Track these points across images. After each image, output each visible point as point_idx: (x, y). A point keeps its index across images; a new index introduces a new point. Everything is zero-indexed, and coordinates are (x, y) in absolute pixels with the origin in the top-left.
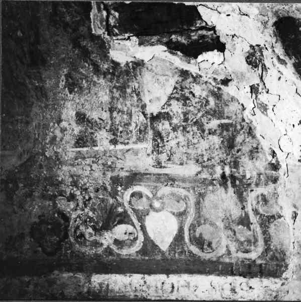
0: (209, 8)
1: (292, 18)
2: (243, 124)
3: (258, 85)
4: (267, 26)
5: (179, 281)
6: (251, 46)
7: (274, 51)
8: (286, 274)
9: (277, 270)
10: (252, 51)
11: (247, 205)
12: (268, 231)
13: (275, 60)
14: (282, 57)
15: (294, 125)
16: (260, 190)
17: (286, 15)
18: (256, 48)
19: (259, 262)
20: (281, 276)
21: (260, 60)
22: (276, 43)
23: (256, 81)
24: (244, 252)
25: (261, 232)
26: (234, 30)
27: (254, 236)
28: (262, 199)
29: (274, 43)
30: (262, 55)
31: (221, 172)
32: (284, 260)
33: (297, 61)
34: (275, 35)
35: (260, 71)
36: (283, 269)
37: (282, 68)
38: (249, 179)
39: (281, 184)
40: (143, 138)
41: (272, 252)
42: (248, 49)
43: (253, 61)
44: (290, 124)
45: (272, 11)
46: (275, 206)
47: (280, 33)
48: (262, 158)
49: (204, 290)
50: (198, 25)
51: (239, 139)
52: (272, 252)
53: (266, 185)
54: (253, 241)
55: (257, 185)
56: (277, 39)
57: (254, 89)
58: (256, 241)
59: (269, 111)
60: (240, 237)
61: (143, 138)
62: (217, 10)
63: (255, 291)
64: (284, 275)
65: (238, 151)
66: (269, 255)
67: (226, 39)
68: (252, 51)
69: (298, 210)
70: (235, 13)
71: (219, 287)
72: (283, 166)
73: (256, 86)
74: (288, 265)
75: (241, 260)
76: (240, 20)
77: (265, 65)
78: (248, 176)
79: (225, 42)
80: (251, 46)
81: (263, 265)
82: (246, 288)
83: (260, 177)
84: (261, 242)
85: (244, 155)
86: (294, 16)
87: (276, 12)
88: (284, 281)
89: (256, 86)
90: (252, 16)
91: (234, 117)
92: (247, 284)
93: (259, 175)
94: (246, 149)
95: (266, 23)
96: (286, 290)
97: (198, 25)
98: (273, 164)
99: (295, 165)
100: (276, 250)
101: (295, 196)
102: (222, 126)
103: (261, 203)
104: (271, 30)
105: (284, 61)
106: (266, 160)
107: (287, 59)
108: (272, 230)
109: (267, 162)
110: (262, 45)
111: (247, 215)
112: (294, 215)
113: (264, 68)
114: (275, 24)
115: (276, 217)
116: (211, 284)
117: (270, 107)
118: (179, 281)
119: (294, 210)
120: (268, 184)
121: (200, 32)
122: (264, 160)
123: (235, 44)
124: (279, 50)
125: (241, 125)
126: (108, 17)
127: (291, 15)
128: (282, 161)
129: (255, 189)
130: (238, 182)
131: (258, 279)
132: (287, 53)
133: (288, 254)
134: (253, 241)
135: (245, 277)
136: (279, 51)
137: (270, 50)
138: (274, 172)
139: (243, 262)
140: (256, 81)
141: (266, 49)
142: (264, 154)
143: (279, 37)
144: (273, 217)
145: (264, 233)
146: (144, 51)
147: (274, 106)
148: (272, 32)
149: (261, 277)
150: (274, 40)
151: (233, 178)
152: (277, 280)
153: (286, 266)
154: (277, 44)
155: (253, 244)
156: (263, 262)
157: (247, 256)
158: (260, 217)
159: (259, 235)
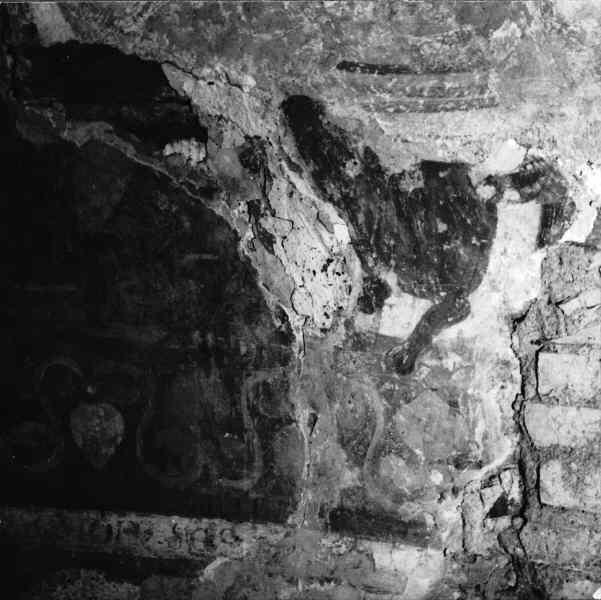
0: (179, 68)
1: (307, 98)
2: (236, 263)
3: (259, 201)
4: (270, 107)
5: (120, 523)
6: (247, 137)
7: (281, 148)
8: (294, 518)
9: (280, 510)
10: (249, 146)
11: (239, 398)
12: (269, 444)
13: (284, 164)
14: (293, 160)
15: (314, 272)
16: (261, 376)
17: (298, 93)
18: (255, 141)
19: (253, 495)
20: (285, 521)
21: (262, 162)
22: (285, 135)
23: (256, 195)
24: (231, 479)
25: (259, 444)
26: (220, 108)
27: (249, 451)
28: (264, 390)
29: (282, 136)
30: (264, 153)
31: (200, 340)
32: (291, 494)
33: (317, 168)
34: (284, 124)
35: (262, 179)
36: (289, 509)
37: (294, 177)
38: (245, 355)
39: (293, 367)
40: (525, 503)
41: (274, 481)
42: (241, 141)
43: (251, 161)
44: (309, 270)
45: (277, 85)
46: (283, 403)
47: (290, 122)
48: (266, 322)
49: (162, 540)
50: (164, 94)
51: (231, 288)
52: (274, 481)
53: (270, 367)
54: (246, 459)
55: (257, 367)
56: (286, 131)
57: (254, 210)
58: (251, 460)
59: (277, 247)
60: (226, 452)
61: (525, 503)
62: (191, 73)
63: (245, 545)
64: (290, 521)
65: (228, 307)
66: (269, 485)
67: (208, 122)
68: (249, 146)
69: (318, 412)
70: (221, 80)
71: (187, 535)
72: (299, 337)
73: (256, 203)
74: (297, 503)
75: (225, 490)
76: (229, 94)
77: (269, 171)
78: (243, 350)
79: (206, 125)
80: (247, 137)
81: (260, 502)
82: (230, 539)
83: (261, 353)
84: (258, 463)
85: (237, 314)
86: (310, 96)
87: (283, 86)
88: (289, 529)
89: (256, 203)
90: (246, 90)
91: (222, 251)
92: (232, 531)
93: (260, 348)
94: (241, 306)
95: (268, 102)
96: (292, 542)
97: (164, 94)
98: (283, 333)
99: (316, 338)
100: (281, 476)
101: (314, 387)
102: (201, 263)
103: (262, 397)
104: (277, 114)
105: (298, 167)
106: (273, 325)
107: (302, 164)
108: (277, 444)
109: (274, 330)
110: (264, 138)
111: (240, 415)
112: (312, 419)
113: (269, 176)
114: (283, 105)
115: (284, 421)
116: (174, 528)
117: (279, 240)
118: (120, 523)
119: (313, 411)
120: (275, 367)
121: (168, 105)
122: (268, 325)
123: (222, 132)
124: (290, 148)
125: (232, 265)
126: (14, 66)
127: (306, 93)
128: (297, 329)
129: (253, 373)
130: (226, 361)
131: (250, 524)
132: (302, 154)
133: (298, 483)
134: (246, 459)
135: (229, 520)
136: (290, 149)
137: (276, 146)
138: (283, 347)
139: (228, 494)
140: (256, 195)
141: (270, 143)
142: (269, 315)
143: (290, 126)
144: (279, 421)
145: (264, 447)
146: (589, 338)
147: (285, 237)
148: (278, 118)
149: (254, 522)
150: (281, 132)
151: (219, 352)
152: (279, 528)
153: (295, 505)
154: (286, 138)
155: (245, 466)
156: (261, 495)
157: (234, 484)
158: (260, 420)
159: (256, 450)
